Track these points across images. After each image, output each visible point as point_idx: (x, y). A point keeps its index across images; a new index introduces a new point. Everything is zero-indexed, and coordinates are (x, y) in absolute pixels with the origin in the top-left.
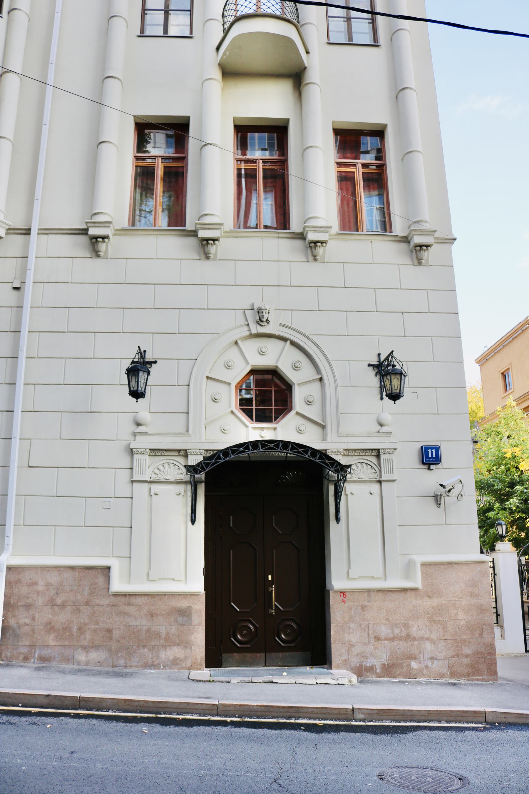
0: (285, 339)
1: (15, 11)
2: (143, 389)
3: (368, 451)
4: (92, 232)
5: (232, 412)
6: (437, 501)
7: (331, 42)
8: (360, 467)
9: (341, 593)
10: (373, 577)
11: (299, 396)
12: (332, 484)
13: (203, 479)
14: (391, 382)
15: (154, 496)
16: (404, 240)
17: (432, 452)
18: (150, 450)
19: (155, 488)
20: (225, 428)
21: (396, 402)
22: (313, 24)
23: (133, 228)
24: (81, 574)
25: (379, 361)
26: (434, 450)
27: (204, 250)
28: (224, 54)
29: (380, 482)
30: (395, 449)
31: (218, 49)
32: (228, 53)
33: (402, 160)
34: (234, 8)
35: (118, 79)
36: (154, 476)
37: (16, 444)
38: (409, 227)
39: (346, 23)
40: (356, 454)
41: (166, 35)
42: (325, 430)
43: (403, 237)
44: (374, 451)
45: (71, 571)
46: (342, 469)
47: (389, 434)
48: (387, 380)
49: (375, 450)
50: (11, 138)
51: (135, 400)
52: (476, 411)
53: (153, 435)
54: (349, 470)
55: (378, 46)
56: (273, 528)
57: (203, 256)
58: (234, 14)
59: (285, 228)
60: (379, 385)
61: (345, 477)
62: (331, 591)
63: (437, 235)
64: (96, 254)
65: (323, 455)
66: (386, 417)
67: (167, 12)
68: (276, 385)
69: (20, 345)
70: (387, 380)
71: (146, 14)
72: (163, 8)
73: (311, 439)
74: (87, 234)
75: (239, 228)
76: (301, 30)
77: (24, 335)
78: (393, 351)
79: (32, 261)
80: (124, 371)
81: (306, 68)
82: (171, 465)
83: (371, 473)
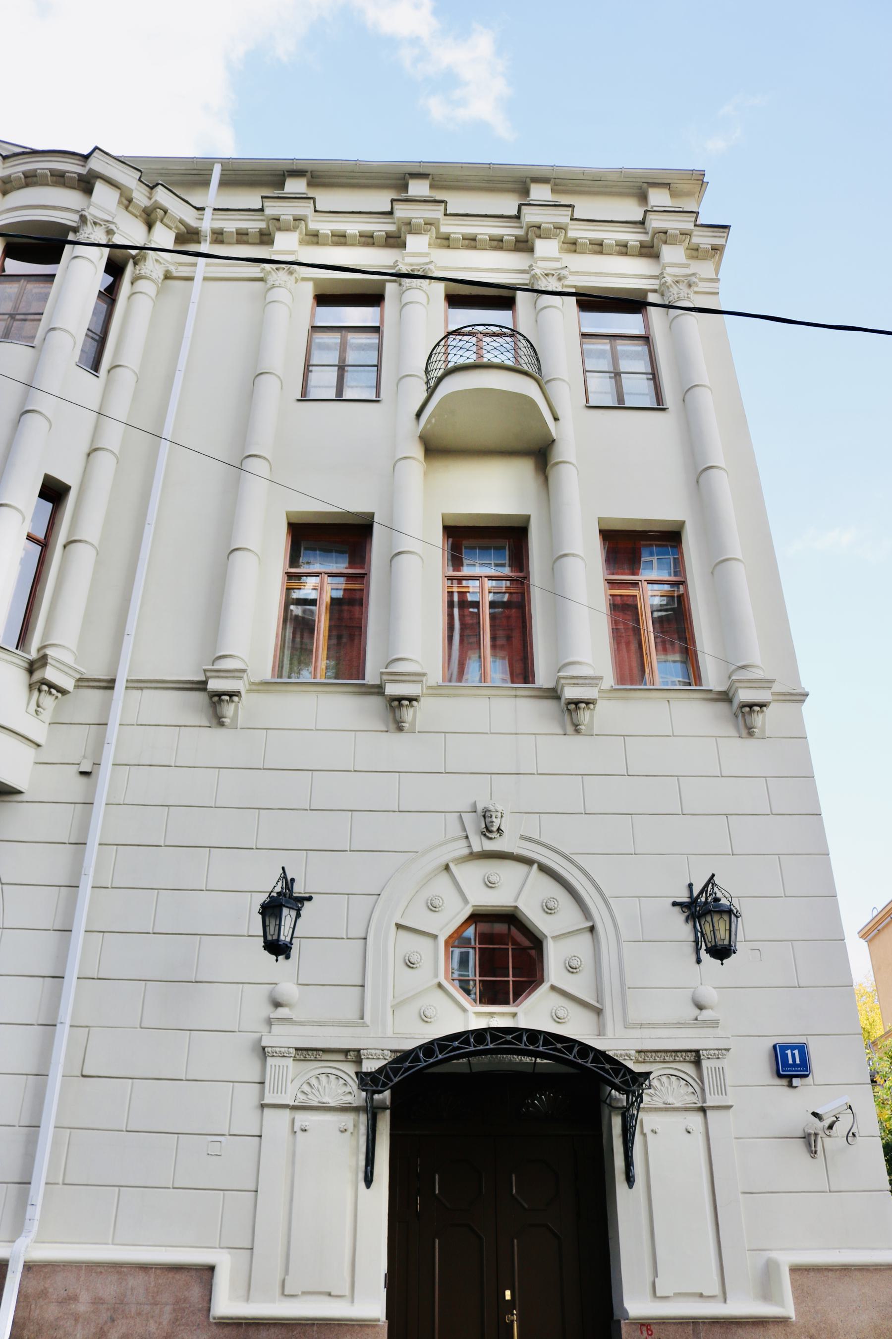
0: (529, 862)
1: (118, 369)
2: (288, 939)
3: (679, 1054)
4: (214, 685)
5: (440, 985)
6: (810, 1145)
7: (590, 404)
8: (666, 1084)
9: (642, 1325)
10: (701, 1295)
11: (554, 958)
12: (617, 1115)
13: (388, 1103)
14: (713, 927)
15: (299, 1133)
16: (723, 697)
17: (793, 1055)
18: (297, 1049)
19: (303, 1119)
20: (427, 1013)
21: (724, 961)
22: (564, 381)
23: (279, 680)
24: (160, 1281)
25: (691, 896)
26: (796, 1052)
27: (395, 716)
28: (428, 421)
29: (703, 1110)
30: (728, 1050)
31: (418, 415)
32: (433, 421)
33: (712, 573)
34: (443, 358)
35: (265, 458)
36: (301, 1097)
37: (63, 1033)
38: (730, 678)
39: (613, 380)
40: (658, 1059)
41: (339, 398)
42: (601, 1017)
43: (720, 693)
44: (689, 1054)
45: (141, 1275)
46: (634, 1082)
47: (714, 1024)
48: (707, 924)
49: (691, 1051)
50: (96, 543)
51: (274, 957)
52: (868, 1027)
53: (301, 1024)
54: (647, 1082)
55: (664, 409)
56: (513, 1196)
57: (392, 726)
58: (443, 366)
59: (526, 681)
60: (692, 938)
61: (640, 1096)
62: (622, 1322)
63: (776, 688)
64: (219, 721)
65: (601, 1056)
66: (709, 994)
67: (342, 368)
68: (515, 942)
69: (85, 865)
70: (707, 924)
71: (311, 371)
72: (337, 363)
73: (577, 1027)
74: (205, 689)
75: (450, 681)
76: (546, 387)
77: (92, 851)
78: (713, 875)
79: (113, 731)
80: (258, 907)
81: (554, 441)
82: (332, 1077)
83: (687, 1094)
